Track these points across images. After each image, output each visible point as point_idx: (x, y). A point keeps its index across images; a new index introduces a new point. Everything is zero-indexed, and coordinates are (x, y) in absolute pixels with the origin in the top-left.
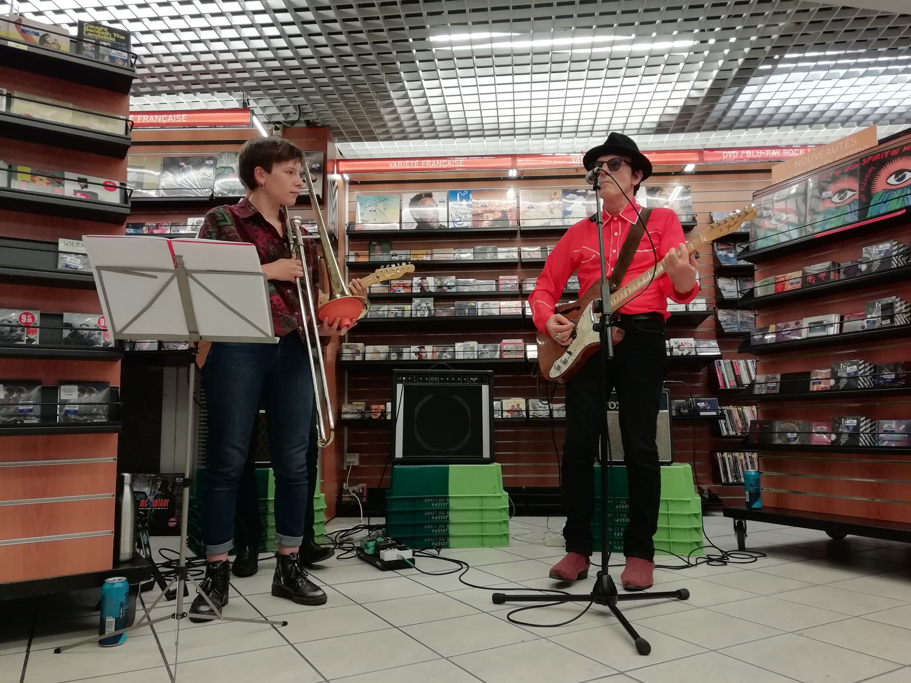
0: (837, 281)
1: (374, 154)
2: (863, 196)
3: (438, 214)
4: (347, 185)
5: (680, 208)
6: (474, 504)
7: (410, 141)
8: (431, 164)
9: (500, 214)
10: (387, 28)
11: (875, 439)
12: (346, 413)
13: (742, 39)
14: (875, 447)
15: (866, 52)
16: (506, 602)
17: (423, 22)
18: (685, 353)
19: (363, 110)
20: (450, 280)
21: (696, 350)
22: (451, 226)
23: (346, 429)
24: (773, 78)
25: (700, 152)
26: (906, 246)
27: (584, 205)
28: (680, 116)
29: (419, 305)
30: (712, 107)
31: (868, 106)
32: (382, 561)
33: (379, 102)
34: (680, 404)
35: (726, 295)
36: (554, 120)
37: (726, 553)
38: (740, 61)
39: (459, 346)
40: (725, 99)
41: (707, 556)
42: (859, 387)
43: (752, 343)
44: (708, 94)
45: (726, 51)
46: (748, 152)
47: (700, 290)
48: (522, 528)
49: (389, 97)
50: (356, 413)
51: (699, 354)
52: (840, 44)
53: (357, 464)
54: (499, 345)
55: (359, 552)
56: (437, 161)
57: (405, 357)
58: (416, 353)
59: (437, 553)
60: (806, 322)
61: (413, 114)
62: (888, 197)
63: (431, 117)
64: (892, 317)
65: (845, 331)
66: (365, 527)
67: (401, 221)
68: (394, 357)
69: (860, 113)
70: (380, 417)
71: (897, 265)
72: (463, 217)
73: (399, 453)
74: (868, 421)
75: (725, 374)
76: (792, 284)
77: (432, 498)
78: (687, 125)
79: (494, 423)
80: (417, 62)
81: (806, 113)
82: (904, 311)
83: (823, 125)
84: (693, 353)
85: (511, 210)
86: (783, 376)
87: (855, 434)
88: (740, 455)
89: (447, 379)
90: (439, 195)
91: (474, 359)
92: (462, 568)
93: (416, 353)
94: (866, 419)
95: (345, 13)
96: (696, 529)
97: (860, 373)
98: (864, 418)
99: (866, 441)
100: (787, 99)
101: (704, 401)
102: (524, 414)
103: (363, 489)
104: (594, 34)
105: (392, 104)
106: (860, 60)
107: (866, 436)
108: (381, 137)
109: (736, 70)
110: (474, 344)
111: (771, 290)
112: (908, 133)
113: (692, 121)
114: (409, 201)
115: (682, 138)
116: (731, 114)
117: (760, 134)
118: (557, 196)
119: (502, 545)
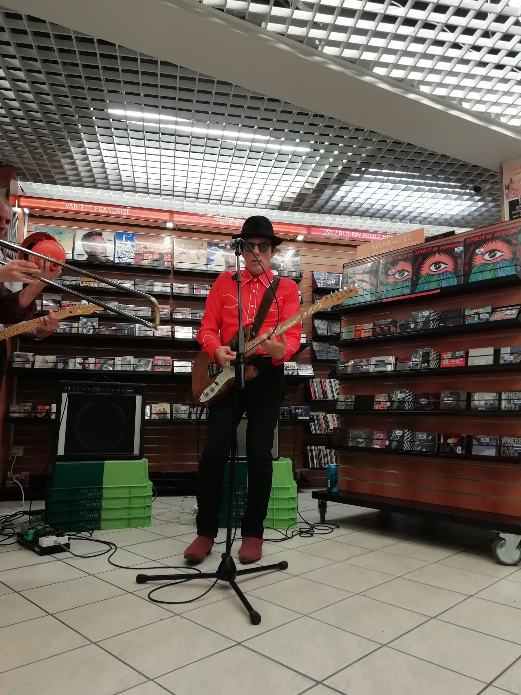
0: (395, 334)
1: (53, 195)
2: (414, 276)
3: (106, 250)
4: (27, 218)
5: (292, 265)
6: (125, 493)
7: (85, 189)
8: (103, 210)
9: (157, 256)
10: (72, 96)
11: (413, 445)
12: (14, 412)
13: (343, 153)
14: (413, 451)
15: (419, 176)
16: (148, 582)
17: (104, 96)
18: (290, 373)
19: (45, 157)
20: (114, 305)
21: (297, 372)
22: (117, 261)
23: (13, 425)
24: (360, 183)
25: (309, 227)
26: (439, 314)
27: (223, 255)
28: (296, 200)
29: (86, 324)
30: (318, 197)
31: (417, 211)
32: (40, 547)
33: (60, 153)
34: (284, 410)
35: (320, 332)
37: (312, 525)
38: (340, 168)
39: (118, 360)
40: (328, 192)
41: (300, 529)
42: (406, 409)
43: (338, 373)
44: (317, 186)
45: (331, 160)
46: (340, 232)
47: (302, 327)
48: (161, 508)
49: (69, 151)
50: (23, 413)
51: (300, 374)
52: (404, 168)
53: (21, 454)
54: (151, 360)
55: (19, 539)
56: (108, 208)
57: (71, 366)
58: (81, 364)
59: (89, 535)
60: (373, 360)
61: (90, 168)
62: (430, 279)
63: (105, 172)
64: (428, 362)
65: (398, 369)
66: (26, 513)
67: (73, 252)
68: (60, 366)
70: (45, 416)
71: (433, 326)
72: (127, 255)
73: (61, 451)
74: (409, 432)
75: (316, 386)
76: (366, 332)
77: (88, 489)
78: (301, 207)
79: (143, 421)
80: (96, 127)
81: (379, 210)
82: (435, 359)
83: (389, 219)
84: (296, 374)
85: (166, 254)
86: (356, 397)
87: (401, 441)
88: (323, 448)
89: (107, 390)
90: (108, 234)
91: (130, 371)
92: (111, 549)
93: (81, 364)
94: (408, 431)
95: (35, 76)
96: (293, 509)
97: (407, 399)
98: (407, 430)
99: (408, 446)
100: (368, 199)
101: (301, 409)
102: (169, 416)
103: (25, 476)
104: (239, 131)
105: (71, 157)
106: (415, 180)
107: (408, 442)
108: (60, 182)
109: (336, 174)
110: (131, 359)
111: (352, 336)
112: (444, 237)
113: (304, 204)
114: (82, 237)
116: (331, 203)
118: (204, 247)
119: (145, 525)
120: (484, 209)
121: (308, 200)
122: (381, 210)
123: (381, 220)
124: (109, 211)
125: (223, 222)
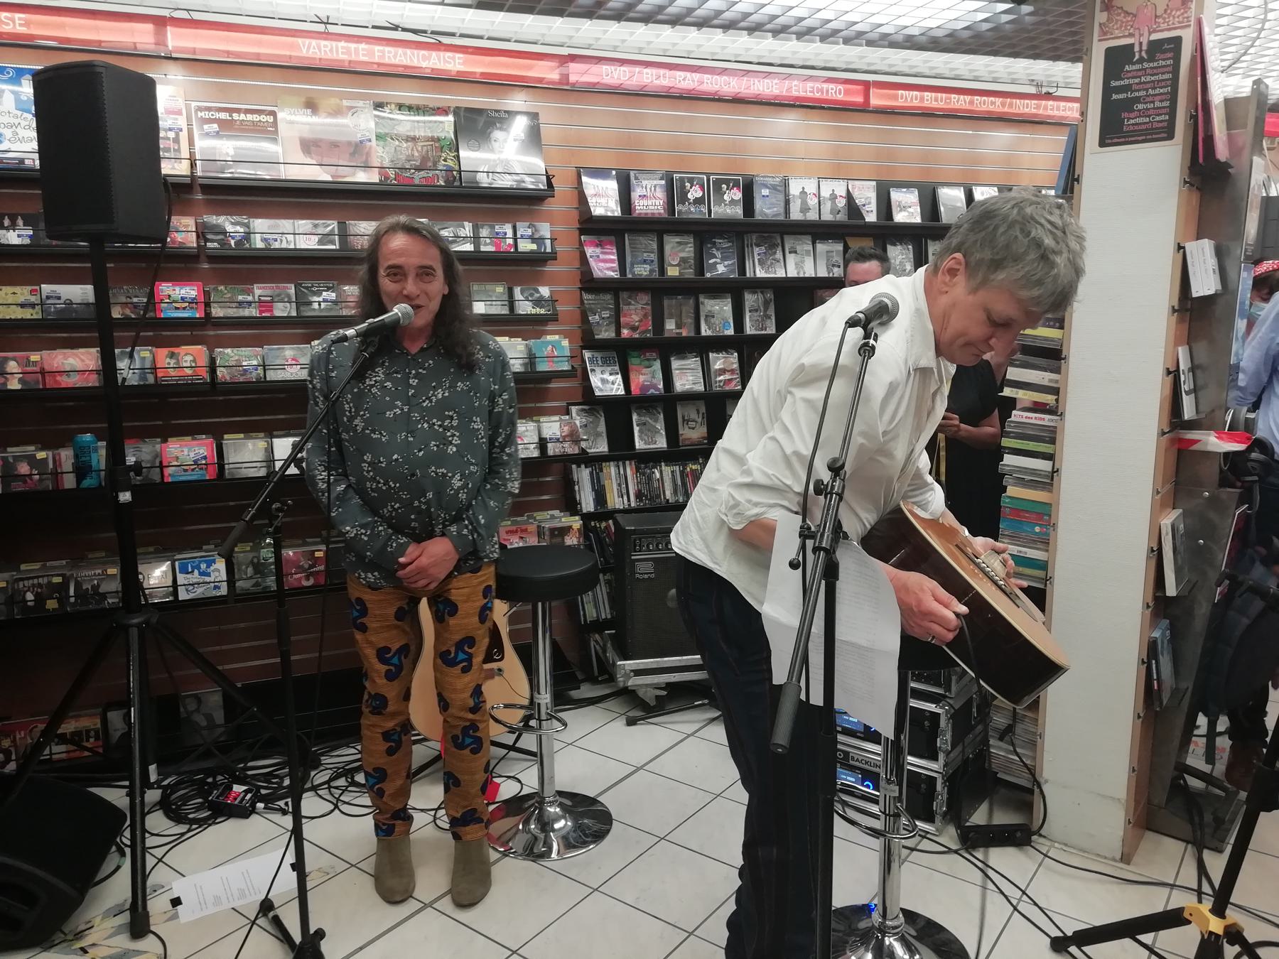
8: (958, 102)
69: (829, 26)
83: (770, 34)
115: (557, 24)
117: (641, 30)
120: (1006, 18)
122: (779, 16)
123: (749, 35)
124: (411, 60)
125: (693, 81)
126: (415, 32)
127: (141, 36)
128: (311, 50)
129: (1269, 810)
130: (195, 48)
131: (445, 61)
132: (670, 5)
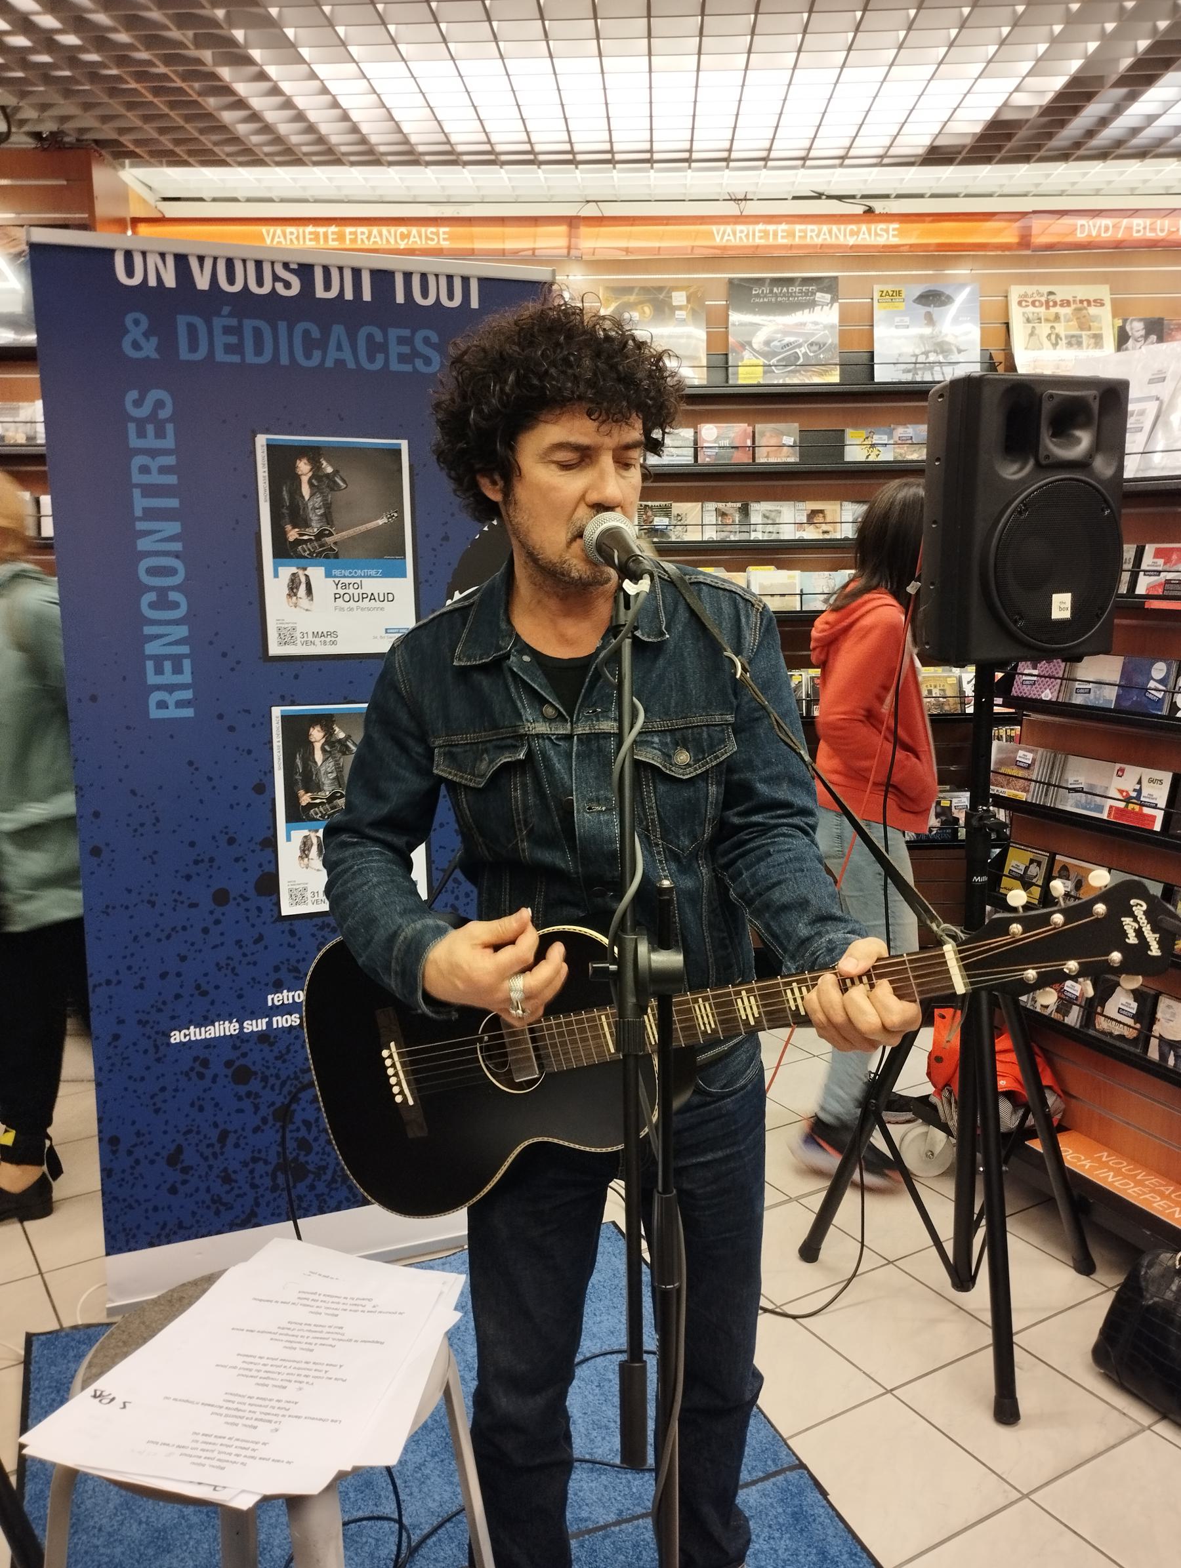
36: (710, 141)
56: (384, 230)
121: (1022, 133)
124: (388, 241)
126: (840, 198)
127: (551, 240)
128: (276, 240)
129: (49, 1122)
130: (504, 250)
131: (876, 234)
132: (1149, 125)
